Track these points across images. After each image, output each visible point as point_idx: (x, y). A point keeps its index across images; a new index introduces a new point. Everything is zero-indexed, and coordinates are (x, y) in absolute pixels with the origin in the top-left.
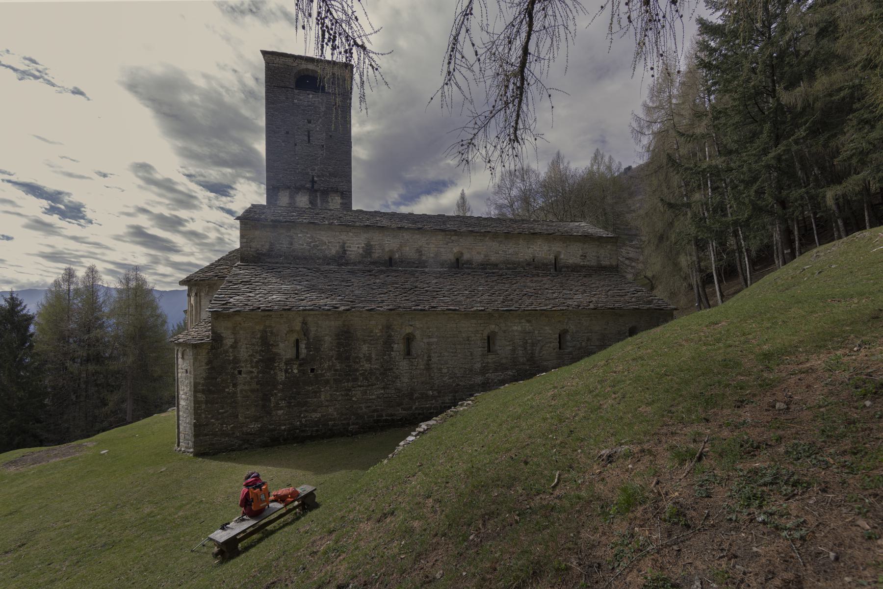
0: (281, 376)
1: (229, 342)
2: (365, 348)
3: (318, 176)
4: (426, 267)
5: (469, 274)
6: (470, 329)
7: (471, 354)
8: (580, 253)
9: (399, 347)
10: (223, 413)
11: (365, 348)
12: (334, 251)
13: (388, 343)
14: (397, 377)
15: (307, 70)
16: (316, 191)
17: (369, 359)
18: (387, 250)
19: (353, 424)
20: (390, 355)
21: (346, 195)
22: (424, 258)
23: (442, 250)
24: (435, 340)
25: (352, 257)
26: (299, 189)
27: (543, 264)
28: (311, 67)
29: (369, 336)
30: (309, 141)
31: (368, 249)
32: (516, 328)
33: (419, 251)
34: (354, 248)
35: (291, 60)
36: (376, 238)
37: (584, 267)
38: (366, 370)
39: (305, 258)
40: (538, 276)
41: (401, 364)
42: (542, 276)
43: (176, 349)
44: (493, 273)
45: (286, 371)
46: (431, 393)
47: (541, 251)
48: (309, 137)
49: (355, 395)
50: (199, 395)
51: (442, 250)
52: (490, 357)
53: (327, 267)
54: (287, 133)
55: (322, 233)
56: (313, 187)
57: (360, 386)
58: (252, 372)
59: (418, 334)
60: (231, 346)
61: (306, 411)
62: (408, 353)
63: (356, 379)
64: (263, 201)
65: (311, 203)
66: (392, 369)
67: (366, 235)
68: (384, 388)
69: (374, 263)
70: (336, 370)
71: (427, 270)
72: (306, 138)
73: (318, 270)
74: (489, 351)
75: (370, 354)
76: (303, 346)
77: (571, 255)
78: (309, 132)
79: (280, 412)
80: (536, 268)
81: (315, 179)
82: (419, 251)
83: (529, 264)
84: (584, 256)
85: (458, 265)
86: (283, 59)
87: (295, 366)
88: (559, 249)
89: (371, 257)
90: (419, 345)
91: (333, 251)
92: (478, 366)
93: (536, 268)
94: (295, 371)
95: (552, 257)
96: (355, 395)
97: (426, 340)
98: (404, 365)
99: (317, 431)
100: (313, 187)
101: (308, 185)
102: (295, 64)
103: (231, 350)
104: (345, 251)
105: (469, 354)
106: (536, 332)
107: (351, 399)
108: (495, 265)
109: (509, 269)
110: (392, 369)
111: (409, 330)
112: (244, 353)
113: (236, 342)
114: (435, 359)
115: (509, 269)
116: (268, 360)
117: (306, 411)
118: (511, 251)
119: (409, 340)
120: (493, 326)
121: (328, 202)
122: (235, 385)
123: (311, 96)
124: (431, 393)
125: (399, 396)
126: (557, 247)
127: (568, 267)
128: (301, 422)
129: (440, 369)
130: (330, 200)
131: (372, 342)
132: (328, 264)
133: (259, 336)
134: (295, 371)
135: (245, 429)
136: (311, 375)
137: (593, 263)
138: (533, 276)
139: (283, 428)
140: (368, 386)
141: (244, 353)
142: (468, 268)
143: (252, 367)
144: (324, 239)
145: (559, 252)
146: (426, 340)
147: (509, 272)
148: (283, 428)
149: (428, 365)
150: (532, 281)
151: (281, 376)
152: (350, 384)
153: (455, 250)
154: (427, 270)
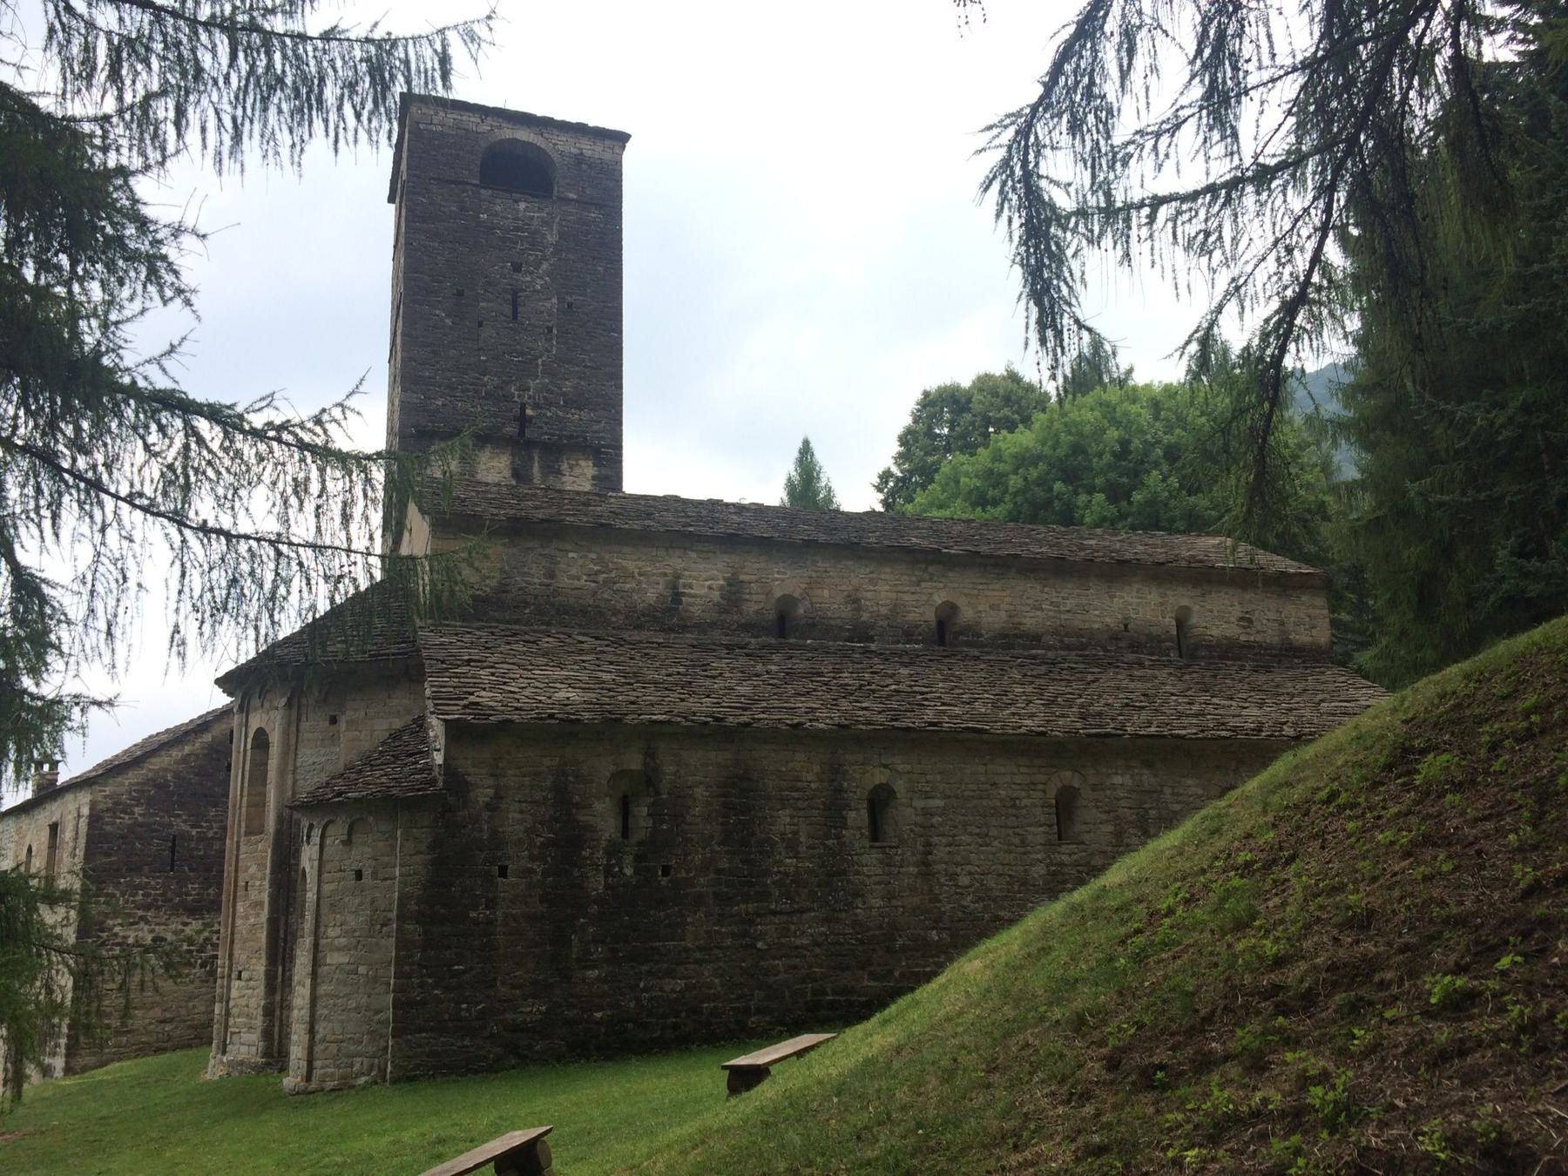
0: (597, 884)
1: (483, 794)
2: (784, 816)
3: (536, 406)
4: (871, 639)
5: (977, 658)
6: (1018, 779)
7: (1023, 843)
8: (1237, 611)
9: (858, 817)
10: (464, 972)
11: (784, 816)
12: (651, 594)
13: (834, 811)
14: (856, 895)
15: (514, 141)
16: (530, 444)
17: (792, 846)
18: (778, 594)
19: (759, 1011)
20: (839, 837)
21: (609, 455)
22: (865, 616)
23: (907, 597)
24: (940, 803)
25: (696, 610)
26: (485, 439)
27: (1150, 637)
28: (524, 135)
29: (792, 789)
30: (515, 318)
31: (734, 592)
32: (1118, 780)
33: (854, 600)
34: (699, 589)
35: (475, 119)
36: (753, 568)
37: (1249, 646)
38: (787, 874)
39: (584, 612)
40: (1141, 665)
41: (865, 859)
42: (1151, 667)
43: (305, 823)
44: (1034, 657)
45: (608, 871)
46: (934, 935)
47: (1144, 607)
48: (515, 305)
49: (761, 936)
50: (409, 927)
51: (907, 597)
52: (1064, 848)
53: (636, 636)
54: (460, 294)
55: (627, 550)
56: (522, 432)
57: (774, 913)
58: (531, 871)
59: (900, 786)
60: (488, 806)
61: (650, 973)
62: (875, 834)
63: (764, 896)
64: (661, 458)
65: (516, 474)
66: (844, 873)
67: (726, 558)
68: (827, 920)
69: (747, 627)
70: (719, 872)
71: (873, 646)
72: (507, 309)
73: (620, 642)
74: (1060, 838)
75: (796, 833)
76: (642, 811)
77: (1218, 617)
78: (515, 293)
79: (593, 974)
80: (1135, 646)
81: (529, 412)
82: (854, 600)
83: (1115, 638)
84: (1246, 621)
85: (946, 634)
86: (452, 117)
87: (628, 859)
88: (1185, 602)
89: (740, 612)
90: (905, 815)
91: (651, 596)
92: (1039, 871)
93: (1135, 646)
94: (629, 871)
95: (1169, 621)
96: (761, 936)
97: (919, 803)
98: (870, 862)
99: (675, 1027)
100: (522, 432)
101: (511, 429)
102: (485, 128)
103: (485, 815)
104: (677, 597)
105: (1017, 841)
106: (1168, 791)
107: (754, 946)
108: (1035, 639)
109: (1068, 648)
110: (844, 873)
111: (880, 777)
112: (514, 820)
113: (498, 797)
114: (940, 853)
115: (1068, 648)
116: (567, 841)
117: (650, 973)
118: (1070, 604)
119: (880, 801)
120: (1069, 774)
121: (559, 472)
122: (491, 904)
123: (522, 206)
124: (934, 935)
125: (862, 942)
126: (1181, 597)
127: (1210, 647)
128: (638, 1000)
129: (953, 877)
130: (565, 466)
131: (801, 804)
132: (639, 627)
133: (548, 783)
134: (629, 871)
135: (509, 1016)
136: (664, 881)
137: (1271, 637)
138: (1130, 666)
139: (599, 1015)
140: (794, 912)
141: (514, 820)
142: (969, 644)
143: (532, 858)
144: (630, 565)
145: (1187, 609)
146: (919, 803)
147: (1072, 656)
148: (599, 1015)
149: (926, 864)
150: (1132, 678)
151: (597, 884)
152: (751, 907)
153: (938, 599)
154: (873, 646)
